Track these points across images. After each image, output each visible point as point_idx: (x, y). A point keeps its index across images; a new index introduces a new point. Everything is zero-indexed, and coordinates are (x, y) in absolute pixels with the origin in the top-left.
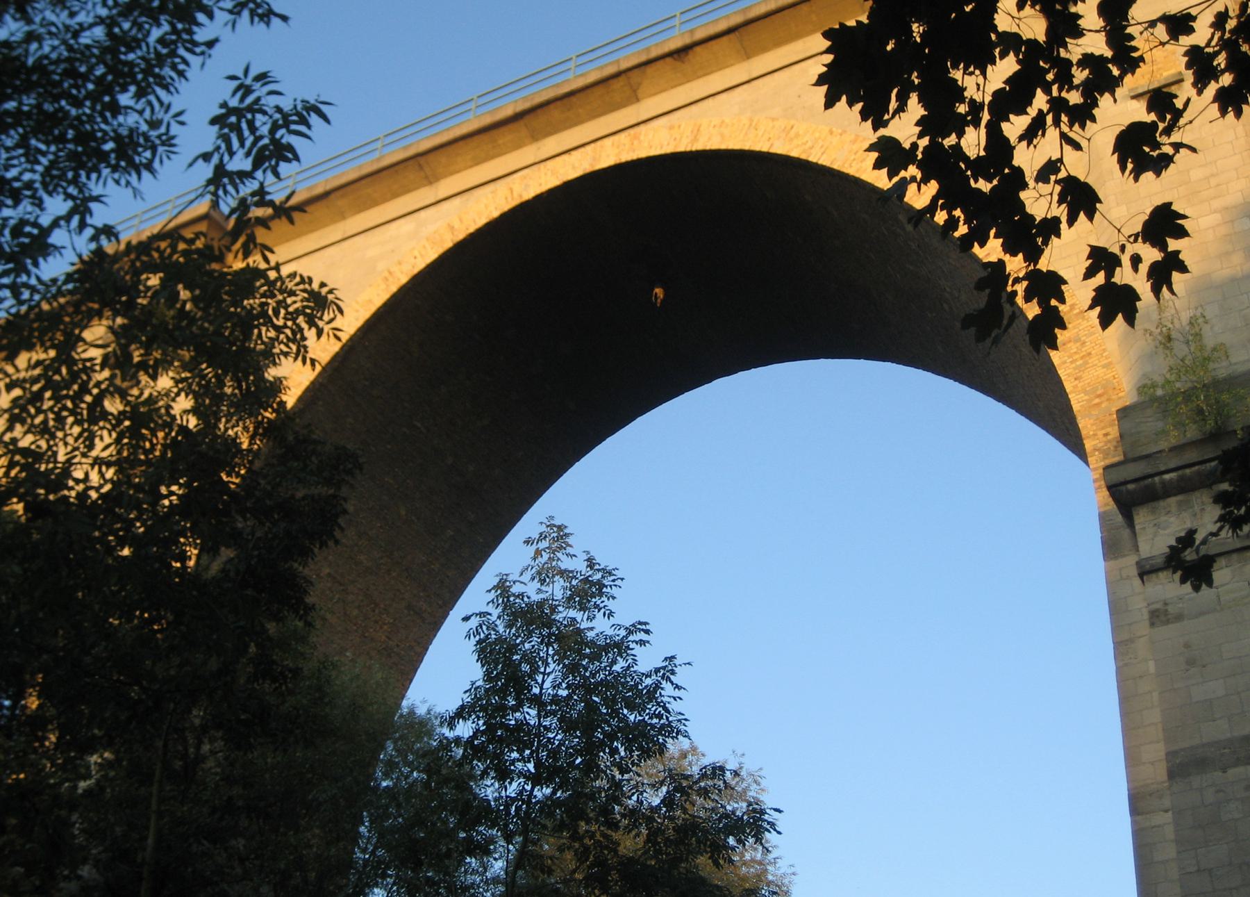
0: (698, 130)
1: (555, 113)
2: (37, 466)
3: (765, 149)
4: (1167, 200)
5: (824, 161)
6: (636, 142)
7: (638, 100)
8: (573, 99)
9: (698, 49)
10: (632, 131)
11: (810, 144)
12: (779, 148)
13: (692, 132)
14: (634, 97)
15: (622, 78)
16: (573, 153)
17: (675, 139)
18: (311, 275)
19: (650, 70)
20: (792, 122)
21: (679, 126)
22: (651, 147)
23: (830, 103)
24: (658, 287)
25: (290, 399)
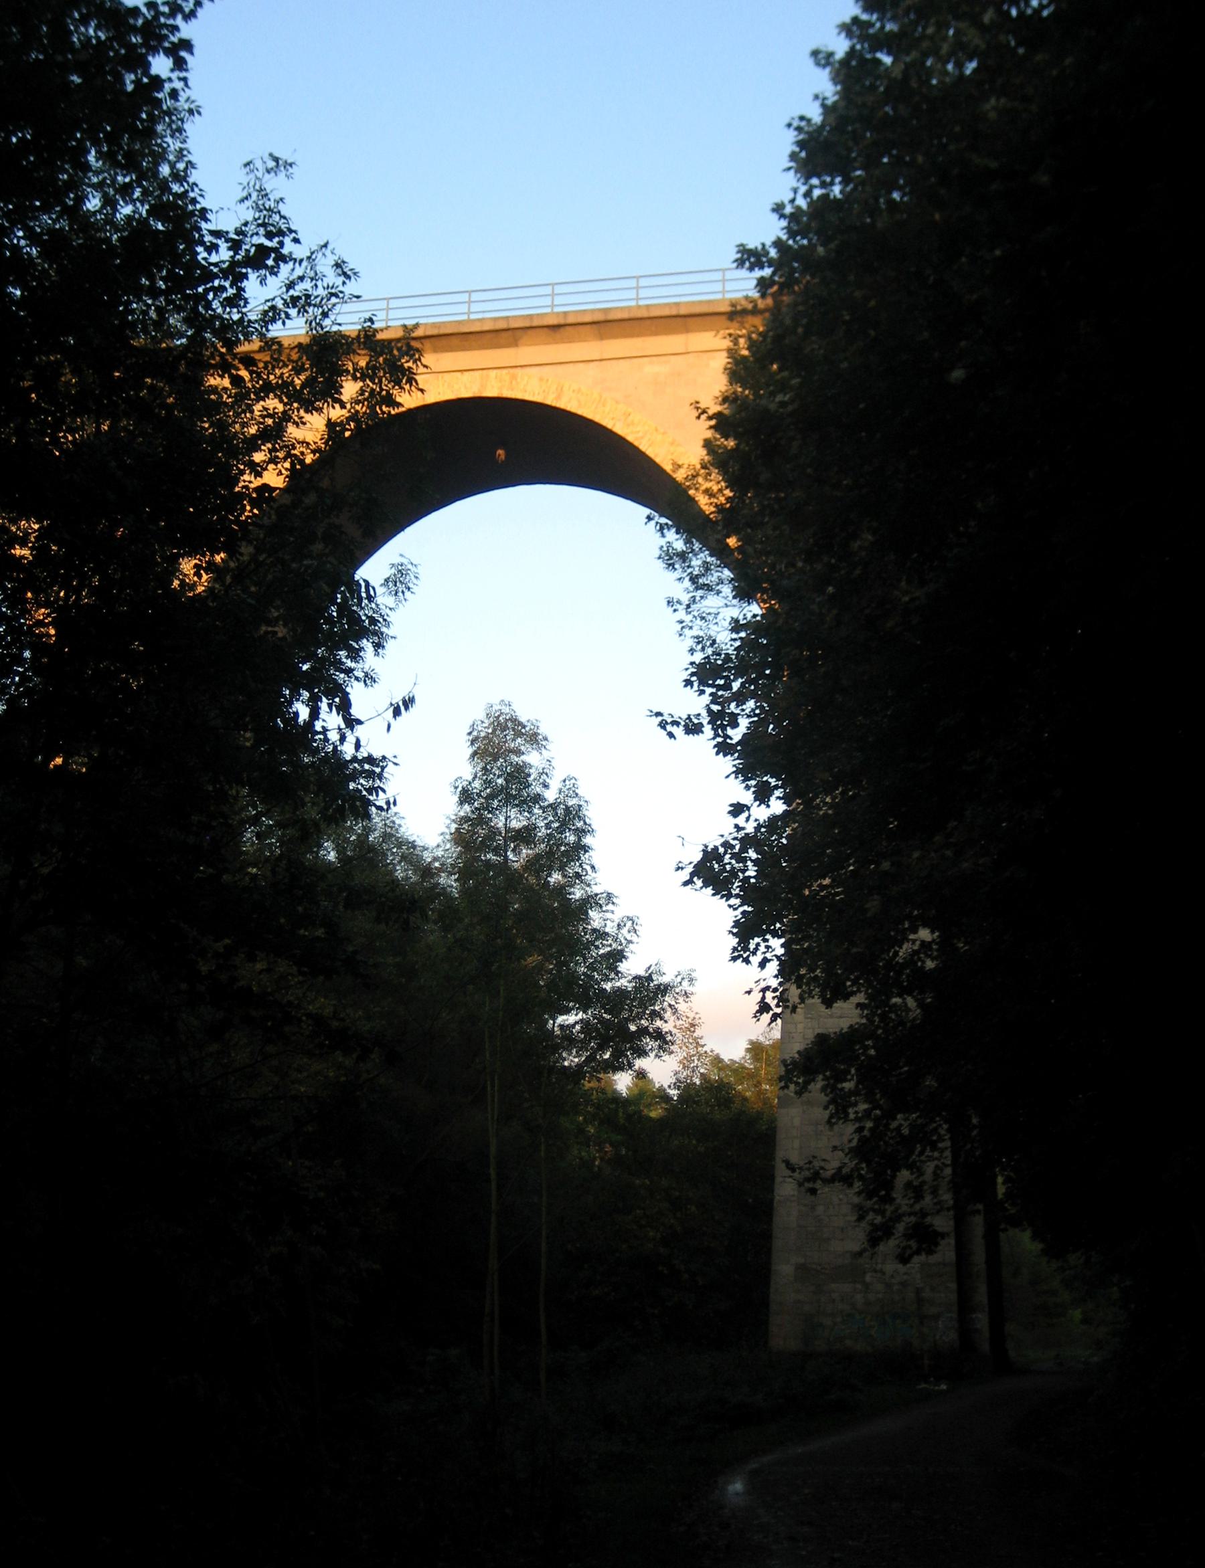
0: (562, 389)
1: (455, 341)
2: (301, 665)
3: (609, 426)
4: (765, 970)
5: (650, 452)
6: (514, 382)
7: (516, 345)
8: (471, 336)
9: (567, 328)
10: (512, 371)
11: (640, 434)
12: (619, 429)
13: (557, 389)
14: (514, 343)
15: (510, 332)
16: (465, 373)
17: (544, 391)
18: (511, 700)
19: (530, 332)
20: (630, 410)
21: (548, 380)
22: (526, 391)
23: (717, 753)
24: (501, 449)
25: (1080, 1310)
